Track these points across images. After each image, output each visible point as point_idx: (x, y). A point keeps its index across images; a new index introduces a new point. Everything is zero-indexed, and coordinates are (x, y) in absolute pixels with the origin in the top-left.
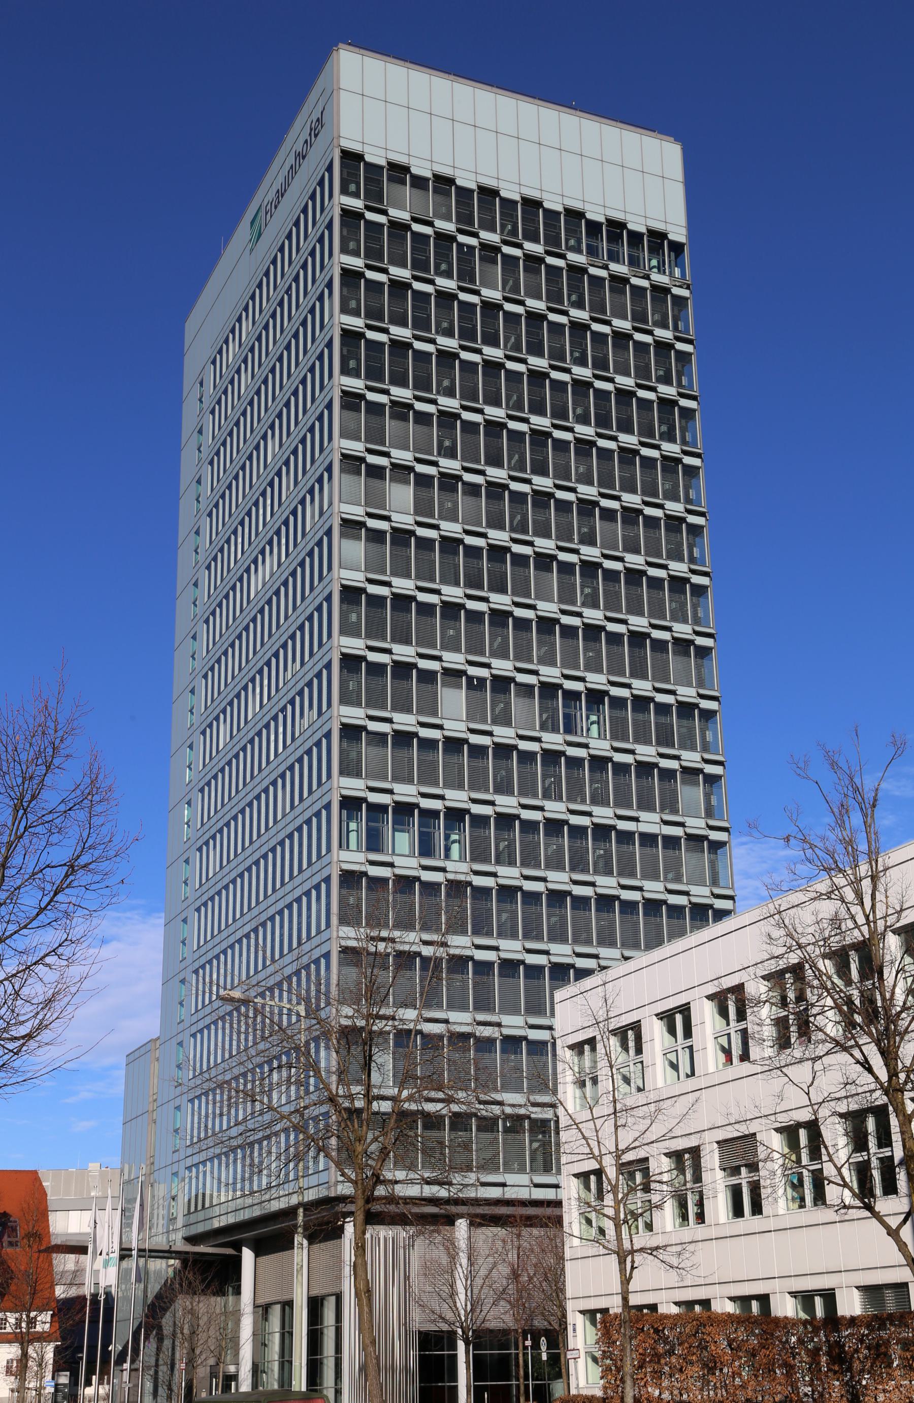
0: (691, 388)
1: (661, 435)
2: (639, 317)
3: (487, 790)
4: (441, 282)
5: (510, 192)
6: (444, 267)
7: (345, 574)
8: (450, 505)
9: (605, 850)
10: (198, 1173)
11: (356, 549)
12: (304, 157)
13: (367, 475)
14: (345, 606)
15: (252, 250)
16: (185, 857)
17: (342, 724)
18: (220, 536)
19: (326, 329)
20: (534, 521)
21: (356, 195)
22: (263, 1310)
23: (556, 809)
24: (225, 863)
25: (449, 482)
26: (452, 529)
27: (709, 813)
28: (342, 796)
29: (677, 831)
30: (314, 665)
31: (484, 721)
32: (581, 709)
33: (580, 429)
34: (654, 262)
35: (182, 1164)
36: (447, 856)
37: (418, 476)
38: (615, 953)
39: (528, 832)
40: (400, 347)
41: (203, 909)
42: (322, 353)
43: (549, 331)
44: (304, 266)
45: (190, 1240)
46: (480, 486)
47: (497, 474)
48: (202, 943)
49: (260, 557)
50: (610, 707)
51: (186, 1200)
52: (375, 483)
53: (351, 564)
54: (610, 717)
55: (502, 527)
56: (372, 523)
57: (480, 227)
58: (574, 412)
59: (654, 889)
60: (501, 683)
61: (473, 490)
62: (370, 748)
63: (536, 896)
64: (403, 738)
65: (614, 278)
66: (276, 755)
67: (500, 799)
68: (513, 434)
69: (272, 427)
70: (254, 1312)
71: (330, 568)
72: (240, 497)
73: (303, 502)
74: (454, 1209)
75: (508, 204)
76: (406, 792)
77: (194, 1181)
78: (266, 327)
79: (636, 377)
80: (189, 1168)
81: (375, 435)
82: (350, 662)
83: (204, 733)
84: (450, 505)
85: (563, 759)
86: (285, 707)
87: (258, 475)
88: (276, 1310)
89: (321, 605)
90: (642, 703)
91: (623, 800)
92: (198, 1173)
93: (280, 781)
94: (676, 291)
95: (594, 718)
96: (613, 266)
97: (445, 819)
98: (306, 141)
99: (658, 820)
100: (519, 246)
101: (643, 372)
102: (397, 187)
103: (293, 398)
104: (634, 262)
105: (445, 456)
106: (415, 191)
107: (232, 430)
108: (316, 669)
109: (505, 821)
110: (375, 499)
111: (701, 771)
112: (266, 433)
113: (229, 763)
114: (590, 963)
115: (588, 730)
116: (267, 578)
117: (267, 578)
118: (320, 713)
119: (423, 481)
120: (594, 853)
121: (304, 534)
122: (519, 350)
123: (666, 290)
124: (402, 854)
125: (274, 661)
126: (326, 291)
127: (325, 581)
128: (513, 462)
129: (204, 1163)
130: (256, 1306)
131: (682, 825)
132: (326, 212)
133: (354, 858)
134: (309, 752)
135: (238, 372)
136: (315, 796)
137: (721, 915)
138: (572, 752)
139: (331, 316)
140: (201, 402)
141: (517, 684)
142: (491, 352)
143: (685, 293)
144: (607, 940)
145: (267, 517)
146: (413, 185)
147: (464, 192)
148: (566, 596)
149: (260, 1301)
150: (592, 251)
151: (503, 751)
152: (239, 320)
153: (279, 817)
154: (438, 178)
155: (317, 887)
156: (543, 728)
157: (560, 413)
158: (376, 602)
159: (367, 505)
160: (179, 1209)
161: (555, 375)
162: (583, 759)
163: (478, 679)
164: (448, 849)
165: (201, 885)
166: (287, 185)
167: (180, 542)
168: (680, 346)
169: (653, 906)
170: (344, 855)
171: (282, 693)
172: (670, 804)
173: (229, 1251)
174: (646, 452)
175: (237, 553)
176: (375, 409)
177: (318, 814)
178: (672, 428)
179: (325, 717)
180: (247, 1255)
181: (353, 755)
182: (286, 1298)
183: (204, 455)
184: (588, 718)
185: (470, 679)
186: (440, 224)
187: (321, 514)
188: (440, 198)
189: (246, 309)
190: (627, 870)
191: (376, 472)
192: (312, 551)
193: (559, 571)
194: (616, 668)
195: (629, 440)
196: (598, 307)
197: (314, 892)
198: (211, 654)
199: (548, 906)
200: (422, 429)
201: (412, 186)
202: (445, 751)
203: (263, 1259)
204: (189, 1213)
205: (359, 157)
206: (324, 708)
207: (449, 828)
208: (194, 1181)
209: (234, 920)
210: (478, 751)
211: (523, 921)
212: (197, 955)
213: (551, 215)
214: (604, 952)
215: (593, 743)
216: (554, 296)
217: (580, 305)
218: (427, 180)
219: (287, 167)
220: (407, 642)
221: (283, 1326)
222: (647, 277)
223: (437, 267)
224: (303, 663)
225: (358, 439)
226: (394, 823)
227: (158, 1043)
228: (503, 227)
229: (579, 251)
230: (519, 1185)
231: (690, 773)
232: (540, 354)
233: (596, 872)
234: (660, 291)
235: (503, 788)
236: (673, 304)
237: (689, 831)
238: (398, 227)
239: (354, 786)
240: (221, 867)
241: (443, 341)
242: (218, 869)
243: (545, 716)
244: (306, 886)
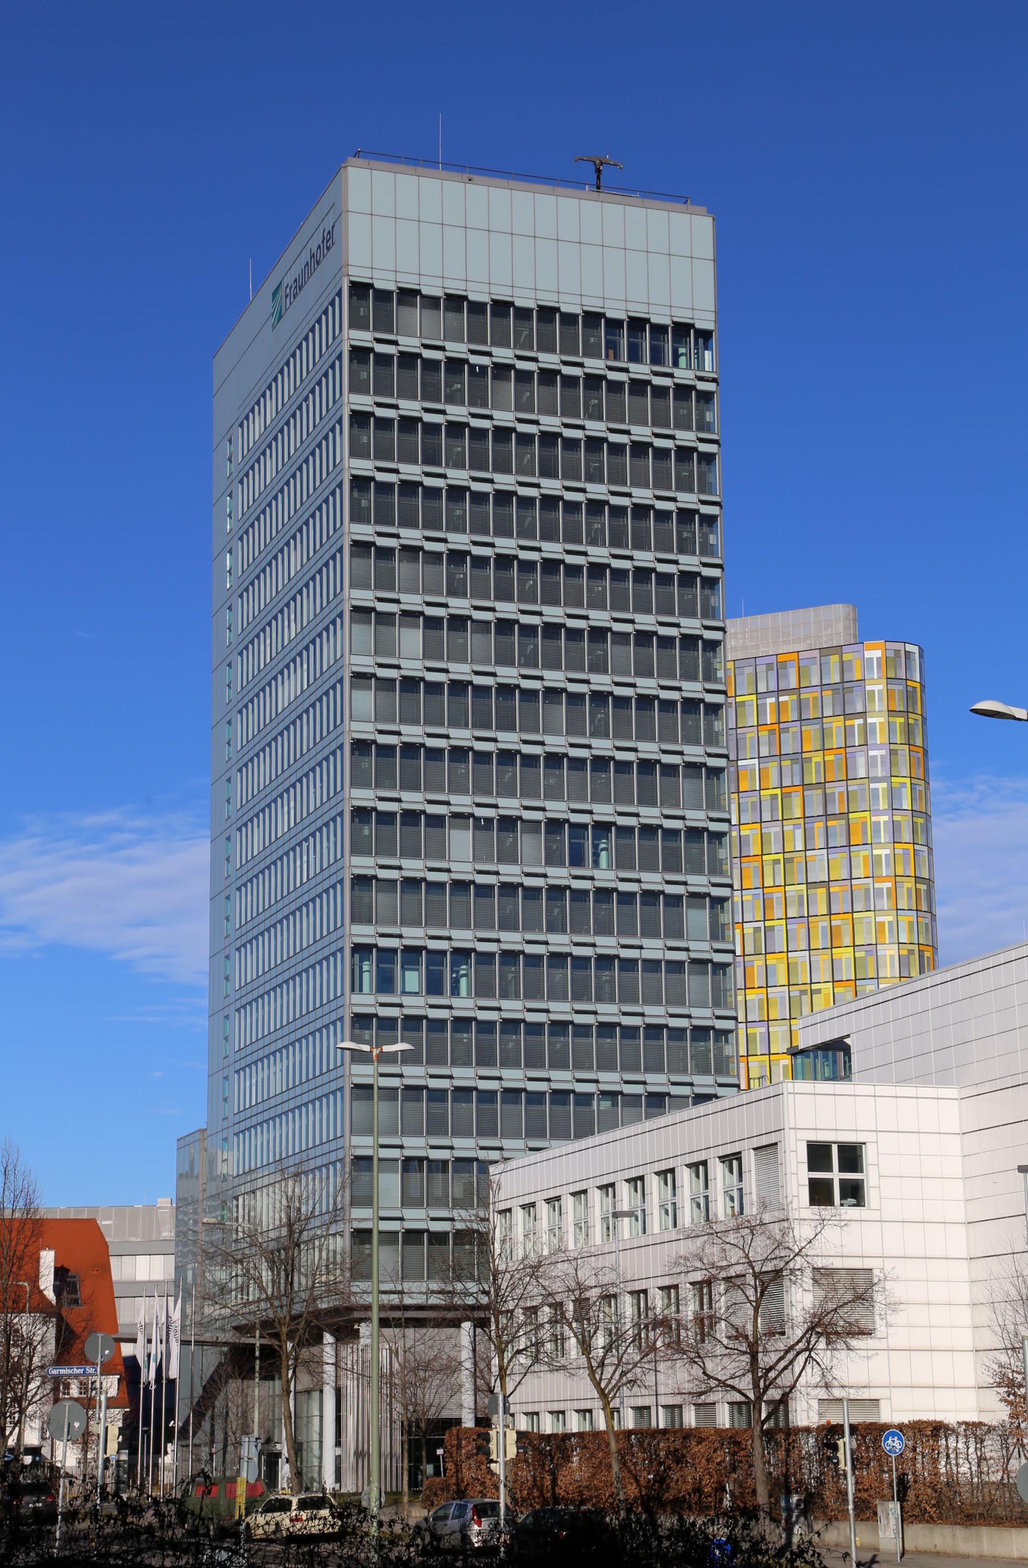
7: (355, 726)
11: (365, 700)
38: (520, 1144)
60: (508, 823)
114: (494, 1155)
124: (412, 996)
170: (356, 998)
185: (477, 819)
191: (385, 619)
207: (455, 965)
214: (507, 1143)
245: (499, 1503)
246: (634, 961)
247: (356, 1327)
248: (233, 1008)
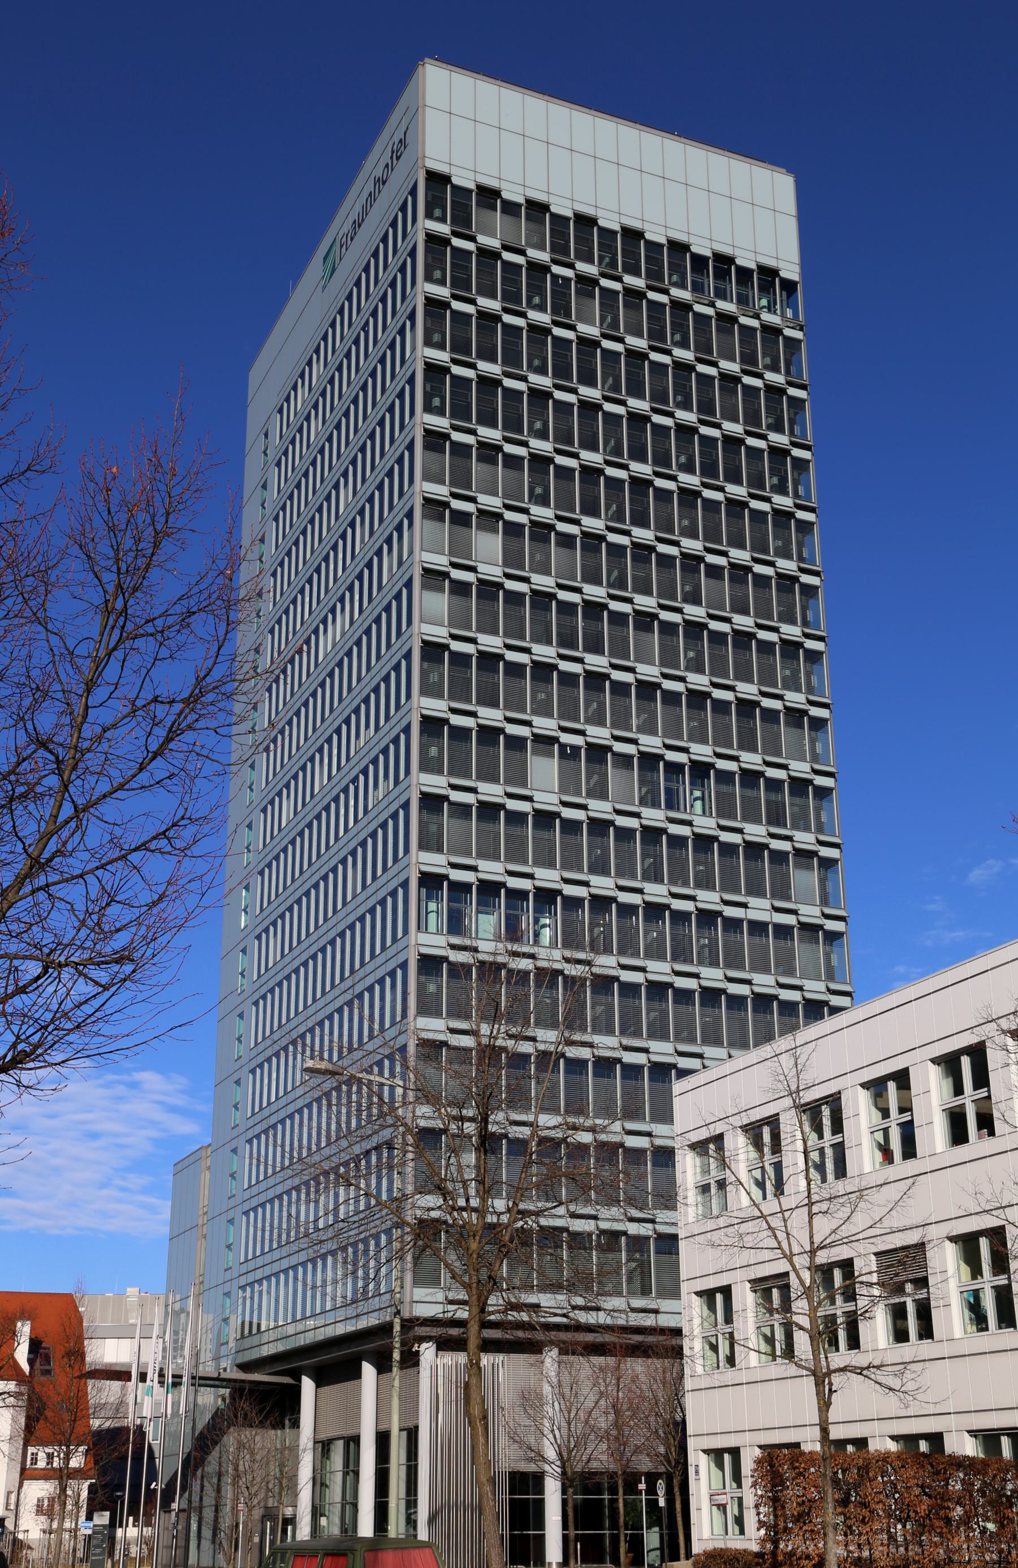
0: (808, 498)
1: (772, 487)
2: (748, 358)
3: (580, 870)
4: (534, 315)
5: (609, 221)
6: (537, 300)
7: (426, 628)
8: (543, 696)
9: (710, 939)
10: (252, 1292)
11: (440, 602)
12: (384, 183)
13: (452, 522)
14: (426, 665)
15: (324, 287)
16: (238, 1011)
17: (422, 793)
18: (285, 596)
19: (407, 430)
20: (634, 577)
21: (442, 282)
22: (324, 1447)
23: (657, 892)
24: (287, 951)
25: (541, 530)
26: (544, 582)
27: (825, 901)
28: (421, 872)
29: (790, 920)
30: (390, 730)
31: (579, 794)
32: (684, 783)
33: (684, 478)
34: (764, 302)
35: (235, 1283)
36: (536, 942)
37: (508, 524)
38: (721, 1052)
39: (627, 996)
40: (488, 384)
41: (261, 1002)
42: (403, 389)
43: (655, 499)
44: (383, 299)
45: (244, 1367)
46: (575, 537)
47: (595, 524)
48: (260, 1039)
49: (330, 616)
50: (717, 781)
51: (239, 1322)
52: (460, 530)
53: (432, 617)
54: (717, 793)
55: (598, 582)
56: (457, 574)
57: (577, 257)
58: (682, 590)
59: (765, 982)
60: (597, 752)
61: (566, 541)
62: (453, 821)
63: (637, 1069)
64: (489, 810)
65: (721, 316)
66: (346, 830)
67: (596, 880)
68: (611, 481)
69: (345, 475)
70: (314, 1449)
71: (410, 622)
72: (309, 551)
73: (379, 553)
74: (540, 1336)
75: (607, 234)
76: (492, 869)
77: (248, 1302)
78: (340, 369)
79: (745, 423)
80: (243, 1288)
81: (461, 479)
82: (431, 725)
83: (264, 810)
84: (543, 696)
85: (664, 837)
86: (356, 778)
87: (328, 527)
88: (339, 1447)
89: (398, 737)
90: (751, 777)
91: (730, 884)
92: (252, 1292)
93: (350, 859)
94: (788, 332)
95: (697, 794)
96: (721, 304)
97: (535, 901)
98: (387, 166)
99: (769, 907)
100: (622, 403)
101: (752, 418)
102: (487, 213)
103: (369, 442)
104: (743, 300)
105: (536, 503)
106: (507, 218)
107: (298, 540)
108: (393, 734)
109: (601, 903)
110: (460, 549)
111: (815, 853)
112: (338, 483)
113: (293, 842)
115: (692, 806)
116: (338, 638)
117: (338, 638)
118: (397, 782)
119: (513, 530)
120: (698, 941)
121: (380, 587)
122: (620, 455)
123: (777, 331)
125: (344, 727)
126: (408, 323)
127: (404, 638)
128: (610, 513)
129: (260, 1281)
130: (315, 1442)
131: (794, 912)
132: (409, 238)
133: (434, 941)
134: (384, 825)
135: (308, 418)
136: (390, 873)
137: (835, 1010)
138: (674, 829)
139: (414, 349)
140: (266, 454)
141: (614, 754)
142: (587, 392)
143: (798, 335)
144: (713, 1038)
145: (339, 572)
146: (504, 211)
147: (559, 220)
148: (669, 658)
149: (322, 1436)
150: (698, 288)
151: (599, 826)
152: (310, 363)
153: (349, 898)
154: (531, 203)
155: (392, 974)
156: (643, 802)
157: (662, 459)
158: (460, 660)
159: (451, 554)
160: (232, 1332)
161: (659, 483)
162: (689, 914)
163: (572, 747)
164: (537, 935)
165: (259, 976)
166: (364, 214)
167: (245, 500)
168: (797, 452)
169: (763, 1001)
170: (423, 938)
171: (353, 762)
172: (781, 890)
173: (287, 1380)
174: (759, 569)
175: (305, 612)
176: (461, 450)
177: (393, 894)
178: (783, 480)
179: (402, 786)
180: (308, 1385)
181: (433, 828)
182: (351, 1432)
183: (268, 511)
184: (691, 794)
185: (563, 747)
186: (533, 253)
187: (400, 563)
188: (533, 226)
189: (317, 351)
190: (734, 961)
191: (461, 519)
192: (389, 605)
193: (660, 632)
194: (722, 738)
195: (738, 491)
196: (704, 347)
197: (388, 980)
198: (271, 786)
199: (648, 999)
200: (512, 473)
201: (503, 211)
202: (535, 826)
203: (325, 1390)
204: (243, 1336)
205: (446, 179)
206: (402, 776)
207: (539, 911)
208: (248, 1302)
209: (297, 1013)
210: (571, 827)
211: (620, 1012)
212: (251, 1122)
213: (654, 247)
214: (709, 1051)
215: (698, 821)
216: (657, 335)
217: (684, 344)
218: (519, 205)
219: (365, 195)
220: (494, 704)
221: (346, 1464)
222: (757, 316)
223: (529, 300)
224: (377, 728)
225: (442, 482)
226: (478, 904)
227: (209, 1150)
228: (601, 258)
229: (683, 286)
230: (616, 1309)
231: (804, 855)
232: (643, 460)
233: (701, 963)
234: (771, 332)
235: (600, 868)
236: (785, 346)
237: (803, 919)
238: (487, 255)
239: (435, 862)
240: (283, 956)
241: (536, 444)
242: (278, 958)
243: (644, 790)
244: (379, 973)
245: (625, 1494)
246: (739, 921)
247: (415, 1348)
248: (239, 1210)
